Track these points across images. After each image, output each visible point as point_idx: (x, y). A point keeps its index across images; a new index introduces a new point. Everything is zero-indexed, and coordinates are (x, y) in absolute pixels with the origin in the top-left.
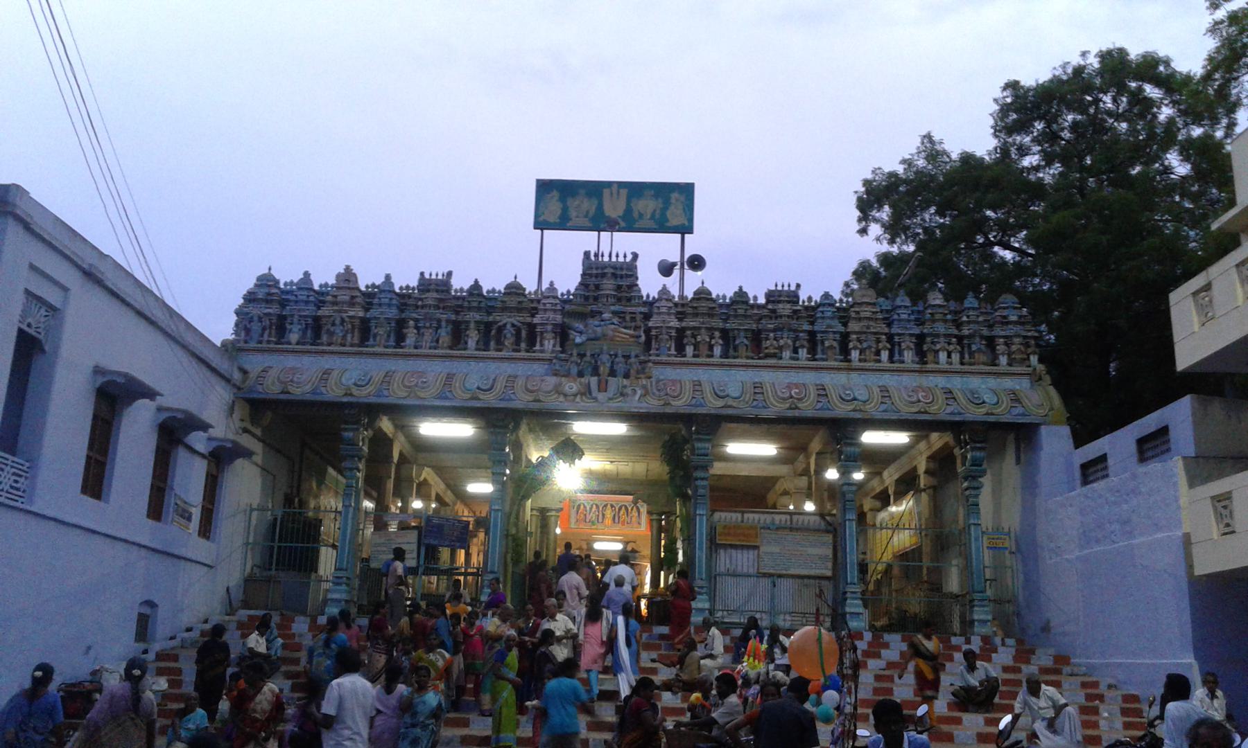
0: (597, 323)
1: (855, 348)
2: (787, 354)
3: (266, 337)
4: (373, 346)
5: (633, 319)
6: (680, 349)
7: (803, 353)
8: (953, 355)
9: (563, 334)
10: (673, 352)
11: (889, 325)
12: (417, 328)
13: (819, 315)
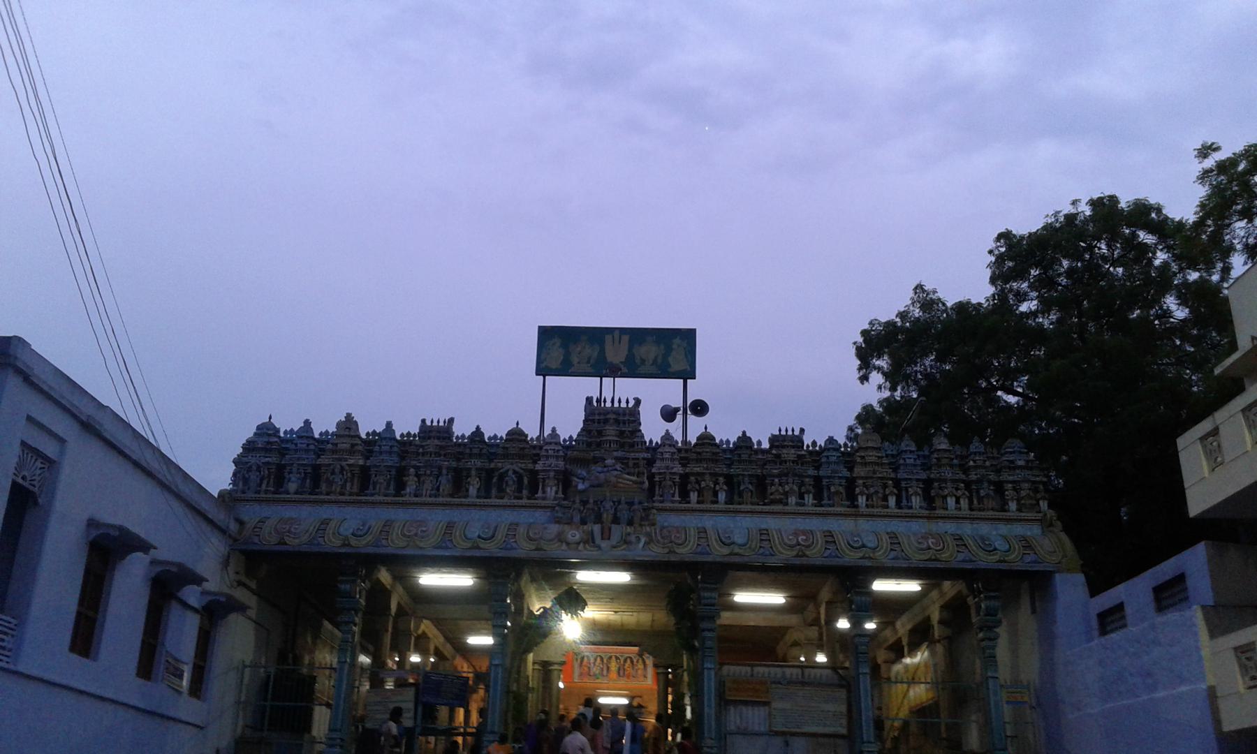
0: (600, 469)
1: (862, 493)
2: (792, 500)
3: (264, 486)
4: (372, 495)
5: (636, 465)
6: (685, 496)
7: (809, 499)
8: (962, 501)
9: (565, 481)
10: (677, 498)
11: (895, 470)
12: (417, 475)
13: (824, 460)
